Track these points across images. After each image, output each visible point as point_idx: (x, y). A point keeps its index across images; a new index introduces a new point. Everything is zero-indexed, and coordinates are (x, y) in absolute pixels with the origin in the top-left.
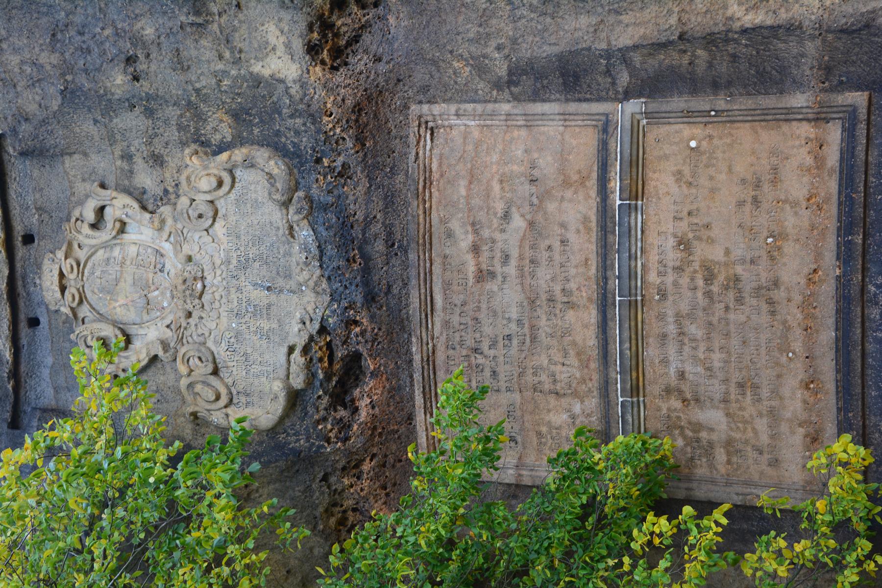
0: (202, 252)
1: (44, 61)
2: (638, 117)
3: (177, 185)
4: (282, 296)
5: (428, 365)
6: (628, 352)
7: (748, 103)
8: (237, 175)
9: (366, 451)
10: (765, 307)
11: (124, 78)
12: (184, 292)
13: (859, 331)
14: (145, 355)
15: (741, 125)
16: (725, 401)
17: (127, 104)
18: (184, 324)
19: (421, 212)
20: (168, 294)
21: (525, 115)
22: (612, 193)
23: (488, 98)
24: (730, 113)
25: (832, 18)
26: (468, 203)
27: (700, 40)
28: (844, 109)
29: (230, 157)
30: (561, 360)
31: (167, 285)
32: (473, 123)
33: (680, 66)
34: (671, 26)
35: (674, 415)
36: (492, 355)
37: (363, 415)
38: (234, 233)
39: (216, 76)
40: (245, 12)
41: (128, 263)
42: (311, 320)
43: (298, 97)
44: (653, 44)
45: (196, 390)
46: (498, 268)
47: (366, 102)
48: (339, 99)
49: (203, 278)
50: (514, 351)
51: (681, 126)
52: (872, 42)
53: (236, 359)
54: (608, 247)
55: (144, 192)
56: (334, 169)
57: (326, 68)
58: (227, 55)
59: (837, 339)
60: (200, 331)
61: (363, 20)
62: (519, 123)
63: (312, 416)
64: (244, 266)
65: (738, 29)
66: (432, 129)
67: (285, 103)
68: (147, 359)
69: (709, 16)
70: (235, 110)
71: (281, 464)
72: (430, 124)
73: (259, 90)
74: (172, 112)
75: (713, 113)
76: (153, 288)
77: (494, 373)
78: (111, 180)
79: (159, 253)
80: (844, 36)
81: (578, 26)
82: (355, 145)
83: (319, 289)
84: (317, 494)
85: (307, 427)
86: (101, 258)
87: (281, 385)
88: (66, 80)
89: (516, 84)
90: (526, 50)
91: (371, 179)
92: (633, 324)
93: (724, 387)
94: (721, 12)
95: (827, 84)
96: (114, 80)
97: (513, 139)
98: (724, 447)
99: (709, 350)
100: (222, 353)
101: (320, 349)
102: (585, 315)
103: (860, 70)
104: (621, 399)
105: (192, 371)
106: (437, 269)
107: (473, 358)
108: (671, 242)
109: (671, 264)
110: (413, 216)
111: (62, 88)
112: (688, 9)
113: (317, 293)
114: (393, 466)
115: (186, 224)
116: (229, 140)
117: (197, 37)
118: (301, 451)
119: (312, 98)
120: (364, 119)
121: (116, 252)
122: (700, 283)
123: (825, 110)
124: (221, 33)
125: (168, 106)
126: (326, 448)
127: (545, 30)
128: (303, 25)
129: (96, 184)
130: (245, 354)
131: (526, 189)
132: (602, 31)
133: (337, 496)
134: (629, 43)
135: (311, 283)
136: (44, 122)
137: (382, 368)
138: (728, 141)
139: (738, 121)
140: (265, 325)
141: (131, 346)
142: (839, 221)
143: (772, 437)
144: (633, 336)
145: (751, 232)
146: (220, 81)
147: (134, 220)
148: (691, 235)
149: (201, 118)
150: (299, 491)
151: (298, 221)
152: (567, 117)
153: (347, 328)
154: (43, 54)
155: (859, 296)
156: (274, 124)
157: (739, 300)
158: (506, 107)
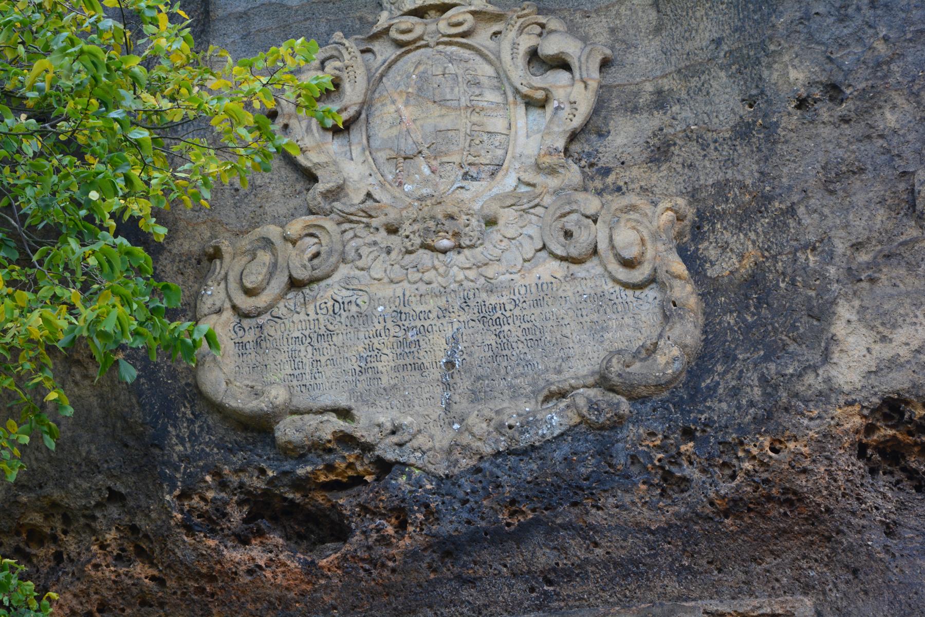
3: (619, 189)
4: (439, 390)
8: (647, 291)
9: (169, 566)
14: (315, 160)
17: (754, 92)
18: (375, 222)
20: (425, 191)
29: (679, 277)
31: (442, 188)
37: (235, 555)
39: (821, 241)
41: (475, 118)
42: (400, 445)
43: (800, 388)
47: (806, 513)
48: (807, 463)
49: (459, 248)
53: (321, 317)
55: (601, 135)
58: (864, 257)
60: (364, 251)
67: (786, 365)
68: (309, 165)
70: (764, 278)
73: (805, 319)
78: (617, 76)
79: (496, 169)
82: (723, 497)
84: (85, 485)
85: (208, 454)
86: (480, 72)
91: (665, 531)
96: (794, 67)
100: (330, 292)
101: (350, 466)
105: (294, 243)
113: (450, 452)
115: (551, 210)
117: (889, 202)
118: (162, 449)
119: (802, 414)
121: (492, 97)
124: (901, 244)
125: (757, 162)
126: (170, 493)
133: (82, 521)
135: (466, 439)
140: (385, 364)
141: (329, 135)
146: (814, 249)
147: (551, 121)
149: (742, 222)
150: (89, 452)
151: (576, 408)
153: (392, 510)
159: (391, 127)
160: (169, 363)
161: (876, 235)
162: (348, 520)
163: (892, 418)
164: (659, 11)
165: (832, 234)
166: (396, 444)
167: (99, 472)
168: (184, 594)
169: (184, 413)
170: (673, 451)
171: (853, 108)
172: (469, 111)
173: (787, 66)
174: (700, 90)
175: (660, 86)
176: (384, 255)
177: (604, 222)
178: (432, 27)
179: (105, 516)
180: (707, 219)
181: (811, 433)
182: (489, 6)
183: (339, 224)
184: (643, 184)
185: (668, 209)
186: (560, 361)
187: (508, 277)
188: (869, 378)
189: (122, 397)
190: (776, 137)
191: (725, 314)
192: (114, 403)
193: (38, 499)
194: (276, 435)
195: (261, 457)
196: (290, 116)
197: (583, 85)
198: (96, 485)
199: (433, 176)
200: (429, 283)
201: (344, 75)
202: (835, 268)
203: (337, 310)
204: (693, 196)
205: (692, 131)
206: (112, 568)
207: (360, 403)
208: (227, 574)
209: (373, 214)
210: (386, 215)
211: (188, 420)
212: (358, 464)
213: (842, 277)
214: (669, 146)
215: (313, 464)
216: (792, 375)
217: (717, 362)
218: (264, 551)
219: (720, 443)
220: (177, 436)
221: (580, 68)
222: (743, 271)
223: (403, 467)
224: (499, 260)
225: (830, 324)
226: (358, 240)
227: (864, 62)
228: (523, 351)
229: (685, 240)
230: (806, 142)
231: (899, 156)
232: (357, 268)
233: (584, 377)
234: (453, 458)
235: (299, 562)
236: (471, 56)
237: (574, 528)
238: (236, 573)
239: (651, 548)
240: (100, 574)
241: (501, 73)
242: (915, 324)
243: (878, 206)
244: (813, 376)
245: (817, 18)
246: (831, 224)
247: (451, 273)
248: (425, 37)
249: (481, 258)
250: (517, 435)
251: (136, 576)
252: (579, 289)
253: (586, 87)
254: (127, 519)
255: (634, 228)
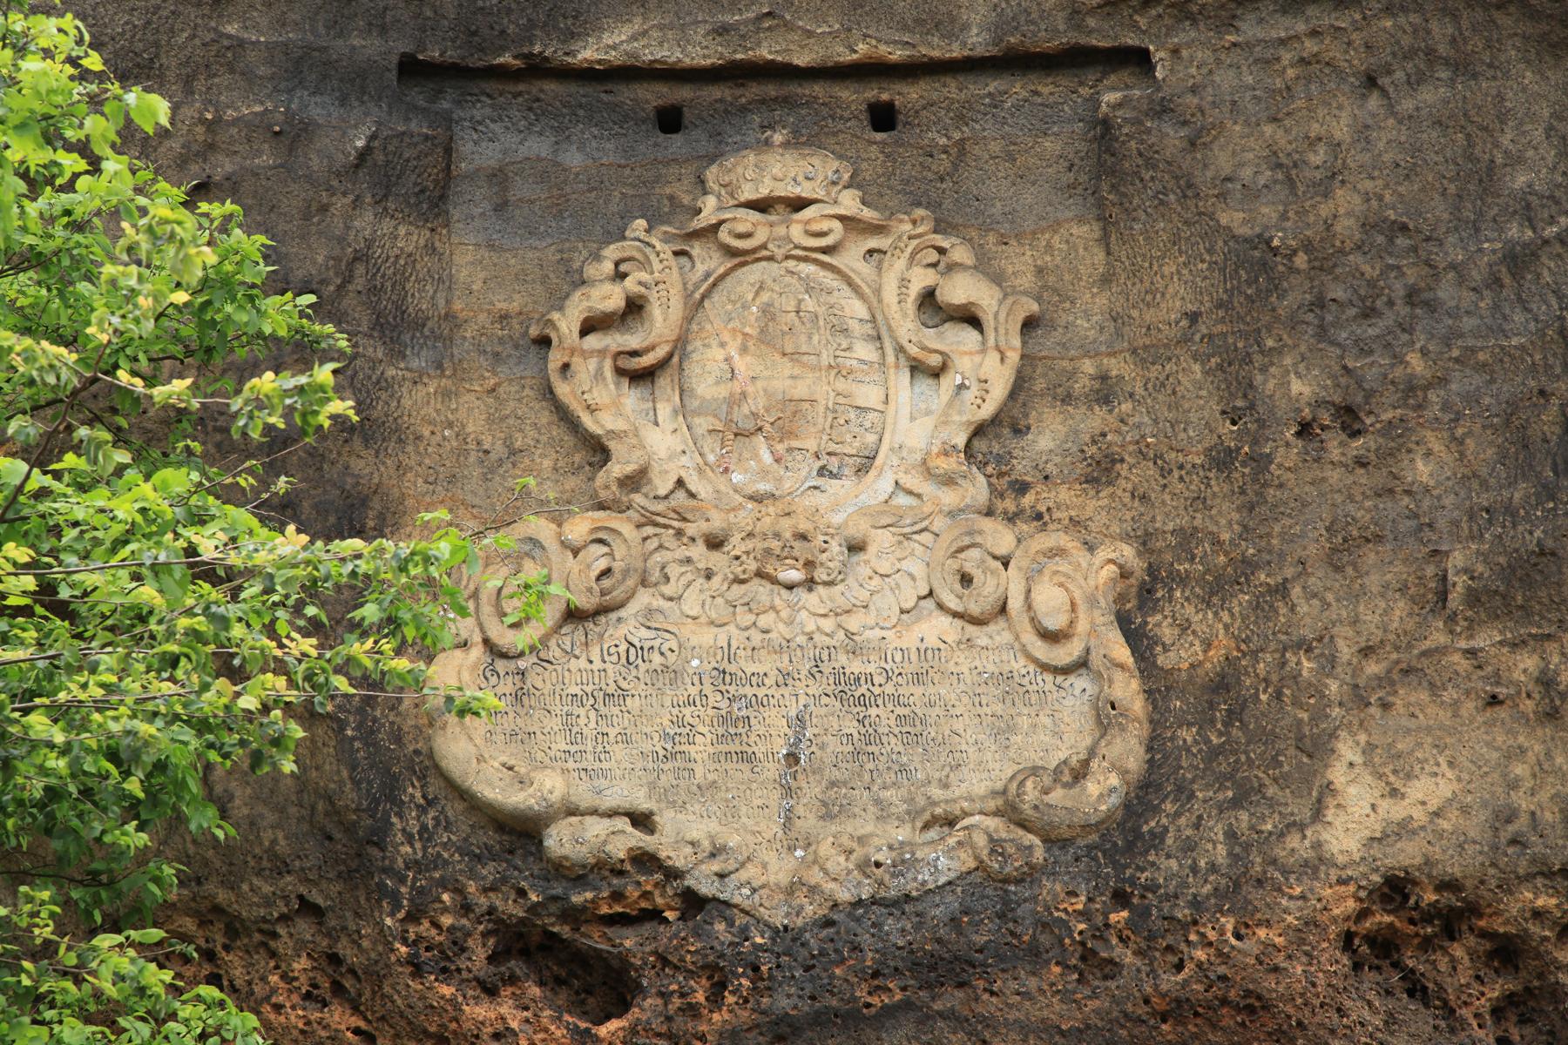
0: (877, 580)
1: (1341, 201)
3: (1039, 516)
4: (776, 794)
8: (1072, 679)
9: (383, 1018)
12: (777, 535)
14: (610, 426)
17: (1240, 403)
18: (691, 529)
29: (1121, 666)
31: (787, 485)
37: (480, 1011)
39: (1320, 639)
40: (1480, 719)
41: (841, 385)
42: (722, 876)
43: (1280, 853)
47: (1271, 1026)
48: (1280, 960)
49: (810, 583)
53: (608, 666)
55: (1019, 431)
56: (1101, 937)
57: (1351, 923)
58: (1373, 668)
60: (674, 570)
61: (1465, 1012)
63: (473, 875)
67: (1263, 818)
68: (599, 431)
70: (1239, 682)
71: (350, 796)
73: (1292, 751)
78: (1047, 343)
79: (866, 464)
82: (1163, 996)
83: (801, 899)
84: (267, 889)
85: (446, 862)
86: (848, 312)
88: (1295, 252)
100: (623, 630)
101: (646, 895)
111: (1276, 242)
113: (790, 891)
115: (946, 539)
116: (1160, 661)
117: (1412, 591)
118: (383, 850)
119: (1280, 890)
120: (1228, 1019)
124: (1424, 654)
125: (1239, 509)
126: (392, 915)
128: (1453, 868)
129: (1035, 307)
130: (624, 694)
133: (257, 937)
135: (815, 876)
136: (1188, 189)
140: (701, 749)
141: (625, 382)
146: (1309, 650)
147: (950, 404)
149: (1212, 594)
150: (274, 842)
151: (973, 847)
154: (1357, 199)
156: (1208, 786)
159: (717, 383)
160: (391, 718)
161: (1392, 637)
162: (636, 970)
163: (1392, 900)
164: (1108, 254)
165: (1335, 631)
166: (716, 874)
167: (288, 872)
169: (412, 796)
171: (1373, 446)
172: (833, 372)
173: (1288, 372)
174: (1163, 385)
175: (1104, 368)
176: (701, 580)
177: (1020, 569)
178: (781, 231)
179: (291, 935)
180: (1162, 581)
181: (1290, 919)
182: (866, 210)
183: (639, 526)
184: (1073, 513)
186: (947, 769)
188: (1371, 847)
189: (327, 767)
190: (1268, 476)
191: (1180, 727)
192: (314, 774)
193: (194, 899)
194: (546, 844)
195: (520, 871)
196: (573, 352)
197: (997, 356)
198: (283, 890)
199: (776, 466)
200: (766, 632)
201: (653, 296)
202: (1338, 683)
203: (632, 659)
204: (1144, 544)
205: (1148, 446)
206: (300, 1013)
207: (663, 805)
208: (465, 1036)
209: (689, 516)
210: (708, 520)
211: (418, 806)
212: (657, 893)
213: (1345, 698)
214: (1114, 462)
215: (595, 888)
216: (1270, 833)
217: (1166, 797)
218: (517, 1007)
219: (1165, 919)
220: (404, 830)
221: (996, 329)
222: (1208, 665)
223: (722, 907)
224: (865, 607)
225: (1326, 766)
226: (664, 552)
227: (1393, 382)
228: (896, 749)
229: (1128, 606)
230: (1307, 489)
231: (1430, 525)
232: (663, 596)
234: (795, 903)
235: (567, 1028)
236: (835, 284)
237: (957, 1019)
238: (477, 1037)
240: (282, 1019)
241: (879, 318)
242: (1436, 774)
243: (1397, 595)
244: (1298, 836)
245: (1334, 307)
246: (1334, 617)
247: (798, 620)
248: (770, 246)
249: (841, 601)
250: (887, 878)
251: (334, 1026)
252: (977, 663)
253: (1002, 360)
254: (324, 944)
255: (1061, 585)
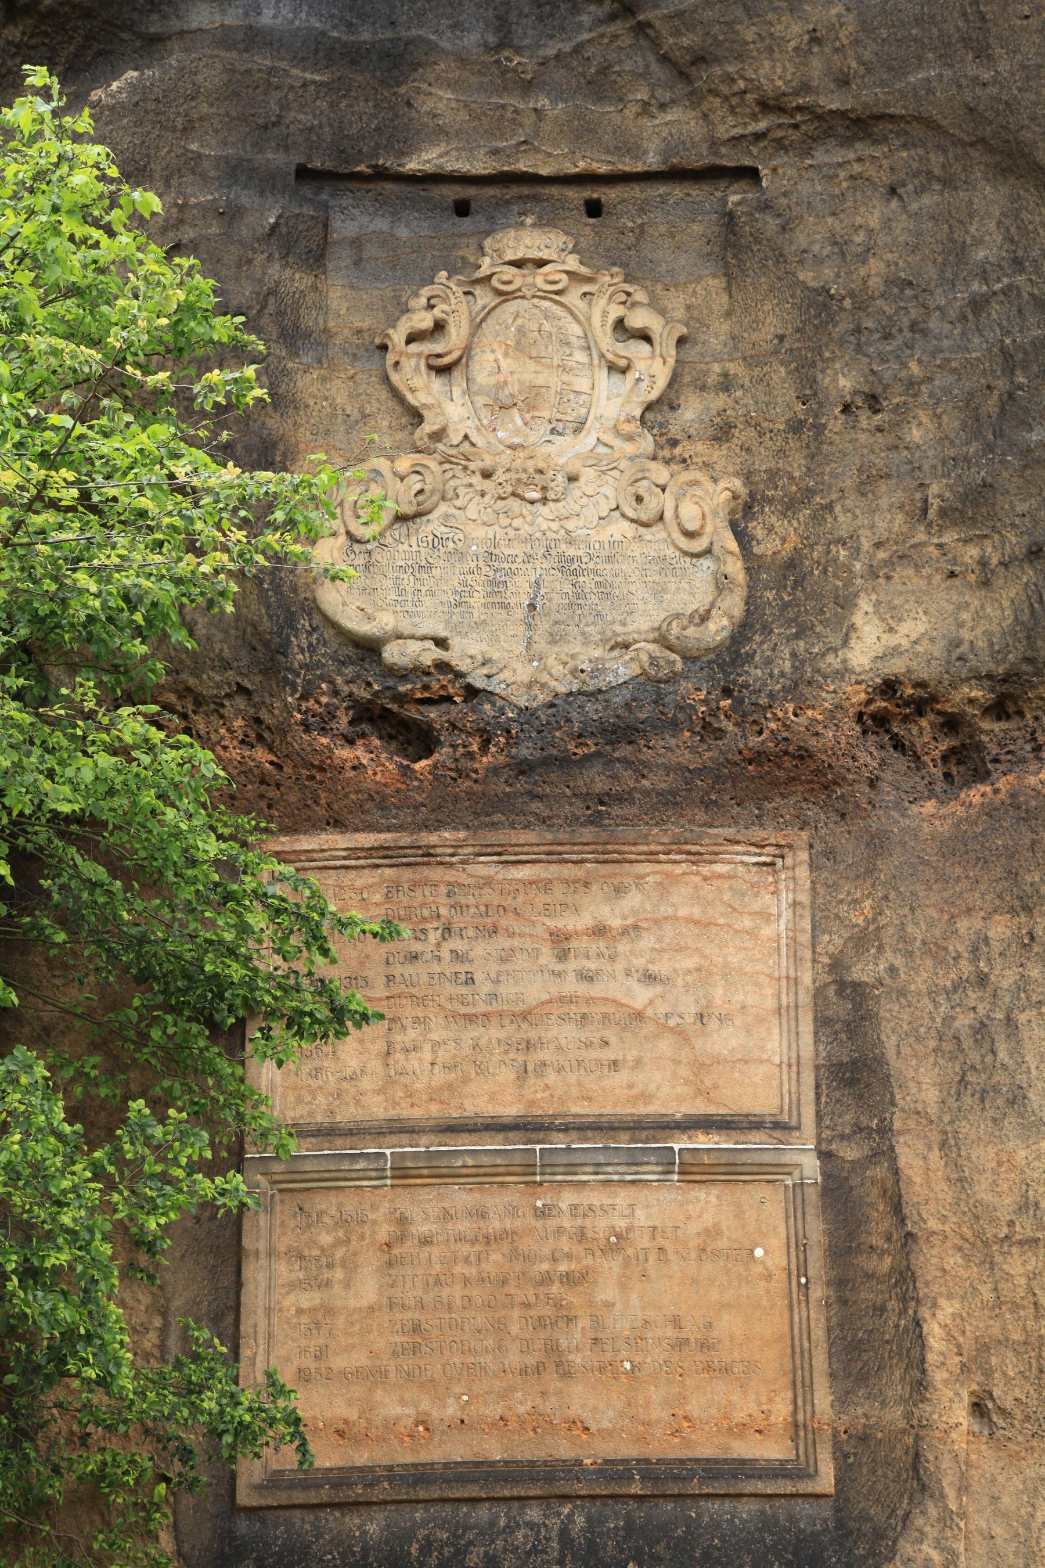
0: (585, 499)
1: (872, 266)
2: (796, 1174)
3: (684, 461)
4: (522, 628)
5: (423, 856)
6: (460, 1163)
7: (819, 1333)
8: (701, 560)
9: (287, 756)
10: (531, 1360)
11: (847, 390)
13: (507, 1493)
15: (787, 1321)
16: (391, 1305)
17: (808, 392)
18: (472, 466)
19: (653, 847)
20: (517, 440)
21: (797, 1007)
22: (690, 1138)
23: (819, 950)
24: (803, 1305)
25: (935, 1442)
26: (666, 918)
27: (905, 1263)
28: (812, 1462)
29: (732, 553)
30: (439, 1061)
32: (783, 927)
33: (869, 1234)
34: (925, 1221)
35: (366, 1229)
36: (442, 955)
37: (344, 753)
38: (614, 553)
39: (851, 537)
41: (565, 377)
42: (489, 677)
43: (822, 666)
44: (900, 1196)
45: (373, 486)
46: (572, 965)
47: (813, 767)
48: (819, 728)
49: (544, 500)
50: (449, 989)
51: (784, 1235)
52: (902, 1495)
54: (612, 1133)
55: (673, 408)
58: (882, 555)
59: (492, 1464)
60: (461, 491)
61: (926, 759)
62: (784, 997)
63: (340, 673)
64: (567, 567)
65: (920, 1314)
66: (772, 864)
67: (813, 645)
68: (416, 404)
69: (938, 1274)
70: (802, 563)
71: (266, 624)
72: (779, 862)
73: (832, 605)
74: (797, 464)
75: (803, 1280)
76: (528, 416)
77: (415, 957)
78: (691, 353)
79: (580, 426)
80: (910, 1459)
81: (924, 1086)
82: (750, 749)
84: (218, 678)
85: (324, 665)
87: (389, 628)
88: (844, 298)
89: (839, 993)
90: (890, 1010)
91: (699, 772)
92: (501, 1170)
93: (412, 1304)
94: (943, 1290)
95: (844, 1437)
96: (844, 375)
97: (760, 986)
98: (322, 1305)
99: (466, 1281)
100: (430, 527)
101: (443, 687)
102: (509, 1097)
103: (864, 1480)
104: (388, 1152)
105: (402, 479)
106: (569, 871)
107: (435, 924)
108: (621, 1224)
109: (588, 1223)
110: (646, 836)
111: (833, 292)
112: (948, 1244)
113: (530, 686)
114: (262, 796)
115: (628, 474)
116: (755, 550)
117: (907, 508)
118: (286, 657)
121: (580, 356)
122: (563, 1267)
123: (810, 1436)
124: (912, 546)
125: (805, 458)
126: (292, 695)
127: (918, 1039)
131: (690, 1008)
132: (919, 1123)
133: (212, 706)
134: (902, 1162)
135: (545, 678)
136: (780, 257)
137: (416, 783)
138: (764, 1303)
139: (792, 1316)
140: (477, 600)
141: (433, 373)
142: (659, 1461)
143: (343, 1373)
144: (482, 1171)
145: (637, 1340)
147: (632, 391)
148: (630, 1252)
149: (788, 509)
150: (221, 650)
152: (794, 1069)
153: (478, 730)
154: (882, 265)
155: (557, 1492)
156: (781, 626)
157: (541, 1323)
158: (807, 978)
165: (860, 532)
168: (297, 779)
170: (714, 705)
178: (530, 280)
181: (826, 705)
183: (441, 463)
185: (727, 489)
187: (585, 531)
192: (245, 610)
200: (517, 530)
201: (451, 320)
214: (731, 427)
215: (413, 683)
231: (919, 468)
233: (646, 632)
239: (687, 784)
241: (589, 336)
244: (833, 656)
245: (866, 332)
